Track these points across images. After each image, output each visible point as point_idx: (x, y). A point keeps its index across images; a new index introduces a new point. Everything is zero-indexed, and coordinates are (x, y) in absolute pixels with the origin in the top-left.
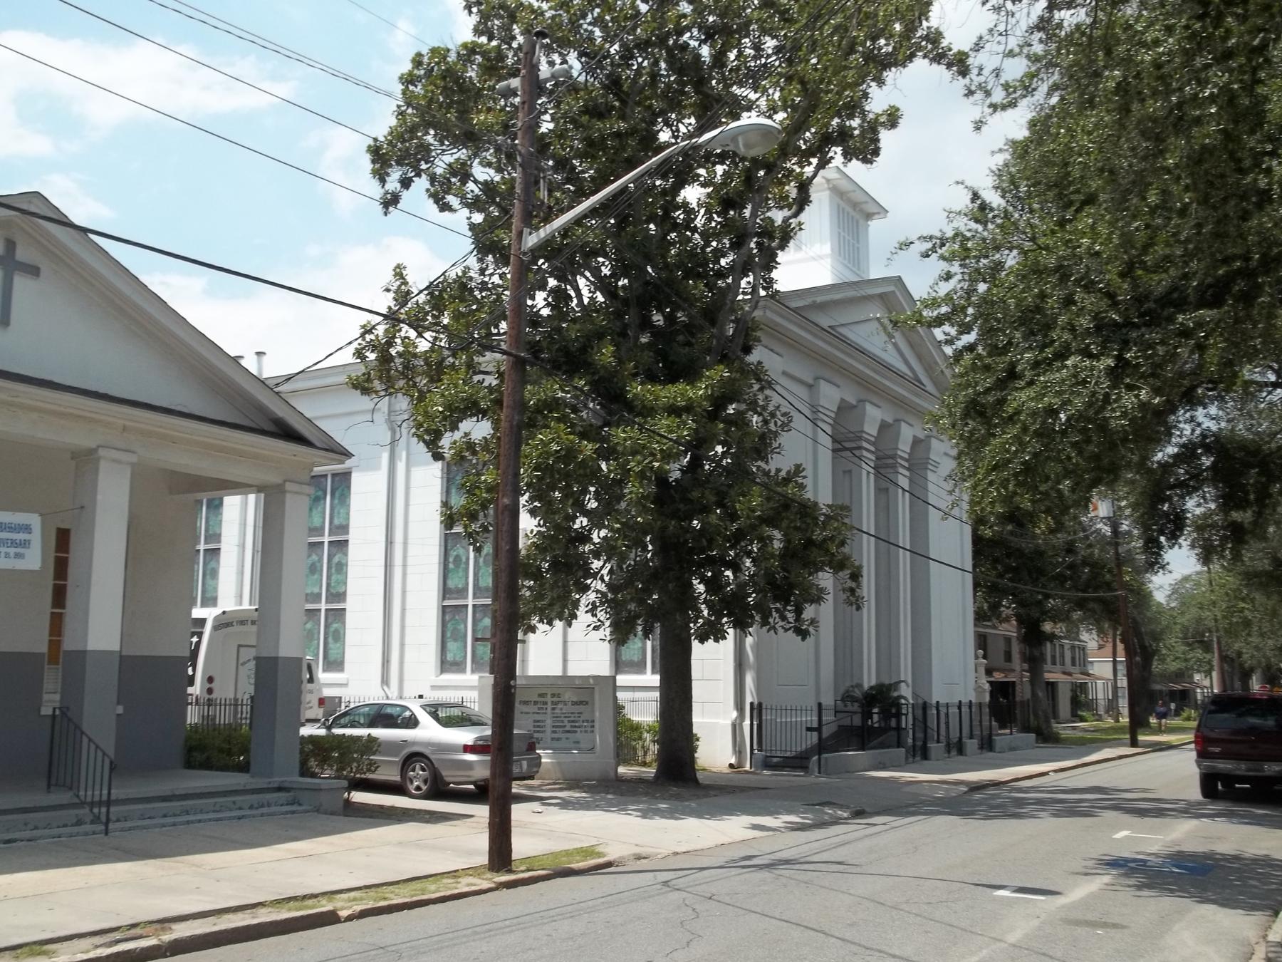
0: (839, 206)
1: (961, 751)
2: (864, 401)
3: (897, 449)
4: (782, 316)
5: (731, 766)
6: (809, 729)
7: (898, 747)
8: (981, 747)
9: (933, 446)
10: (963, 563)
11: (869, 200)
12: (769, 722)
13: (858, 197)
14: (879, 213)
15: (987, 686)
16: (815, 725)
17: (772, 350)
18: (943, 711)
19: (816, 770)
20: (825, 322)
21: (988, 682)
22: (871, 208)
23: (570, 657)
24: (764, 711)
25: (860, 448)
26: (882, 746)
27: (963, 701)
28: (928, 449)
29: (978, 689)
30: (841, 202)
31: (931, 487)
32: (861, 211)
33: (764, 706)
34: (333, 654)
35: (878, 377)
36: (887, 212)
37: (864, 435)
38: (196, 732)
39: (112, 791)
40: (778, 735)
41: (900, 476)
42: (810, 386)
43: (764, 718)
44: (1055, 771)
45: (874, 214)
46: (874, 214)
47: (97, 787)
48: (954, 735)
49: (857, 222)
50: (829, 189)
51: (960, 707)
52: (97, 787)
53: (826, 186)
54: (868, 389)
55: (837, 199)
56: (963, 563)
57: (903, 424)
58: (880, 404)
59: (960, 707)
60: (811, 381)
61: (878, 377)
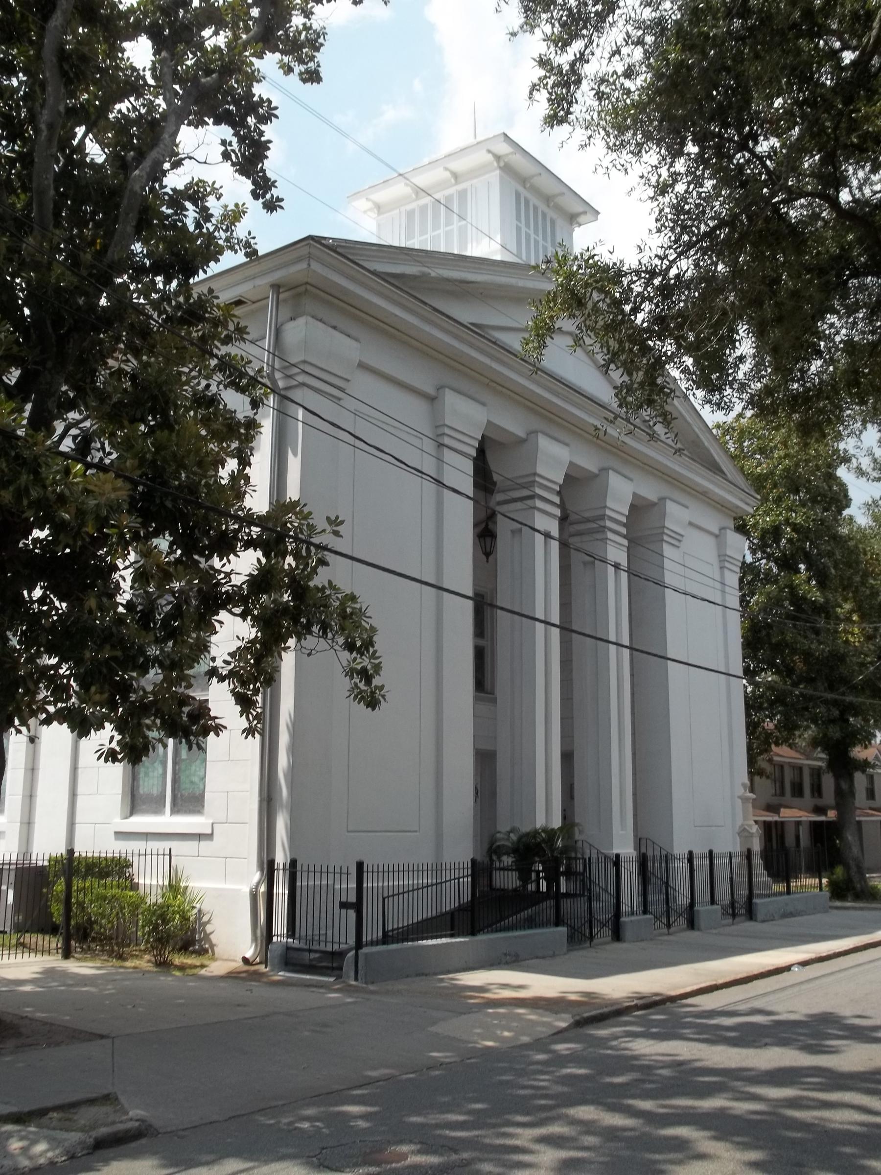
0: (518, 195)
1: (750, 913)
2: (535, 432)
3: (605, 507)
4: (348, 277)
5: (245, 960)
6: (344, 905)
7: (557, 924)
8: (725, 914)
9: (668, 510)
10: (727, 664)
11: (565, 190)
12: (305, 890)
13: (550, 188)
14: (585, 213)
15: (755, 829)
16: (353, 899)
17: (334, 328)
18: (701, 864)
19: (352, 974)
20: (466, 313)
21: (756, 822)
22: (578, 208)
23: (80, 789)
24: (299, 874)
25: (532, 497)
26: (531, 923)
27: (696, 852)
28: (663, 515)
29: (743, 833)
30: (521, 189)
31: (667, 564)
32: (559, 209)
33: (299, 867)
34: (186, 788)
35: (495, 365)
36: (598, 213)
37: (537, 479)
38: (534, 837)
39: (353, 885)
40: (323, 915)
41: (537, 514)
42: (431, 399)
43: (298, 884)
44: (804, 964)
45: (578, 215)
46: (578, 215)
47: (411, 878)
48: (683, 900)
49: (553, 222)
50: (500, 168)
51: (690, 860)
52: (411, 878)
53: (495, 164)
54: (550, 420)
55: (516, 185)
56: (727, 664)
57: (611, 472)
58: (631, 475)
59: (690, 860)
60: (431, 391)
61: (495, 365)
